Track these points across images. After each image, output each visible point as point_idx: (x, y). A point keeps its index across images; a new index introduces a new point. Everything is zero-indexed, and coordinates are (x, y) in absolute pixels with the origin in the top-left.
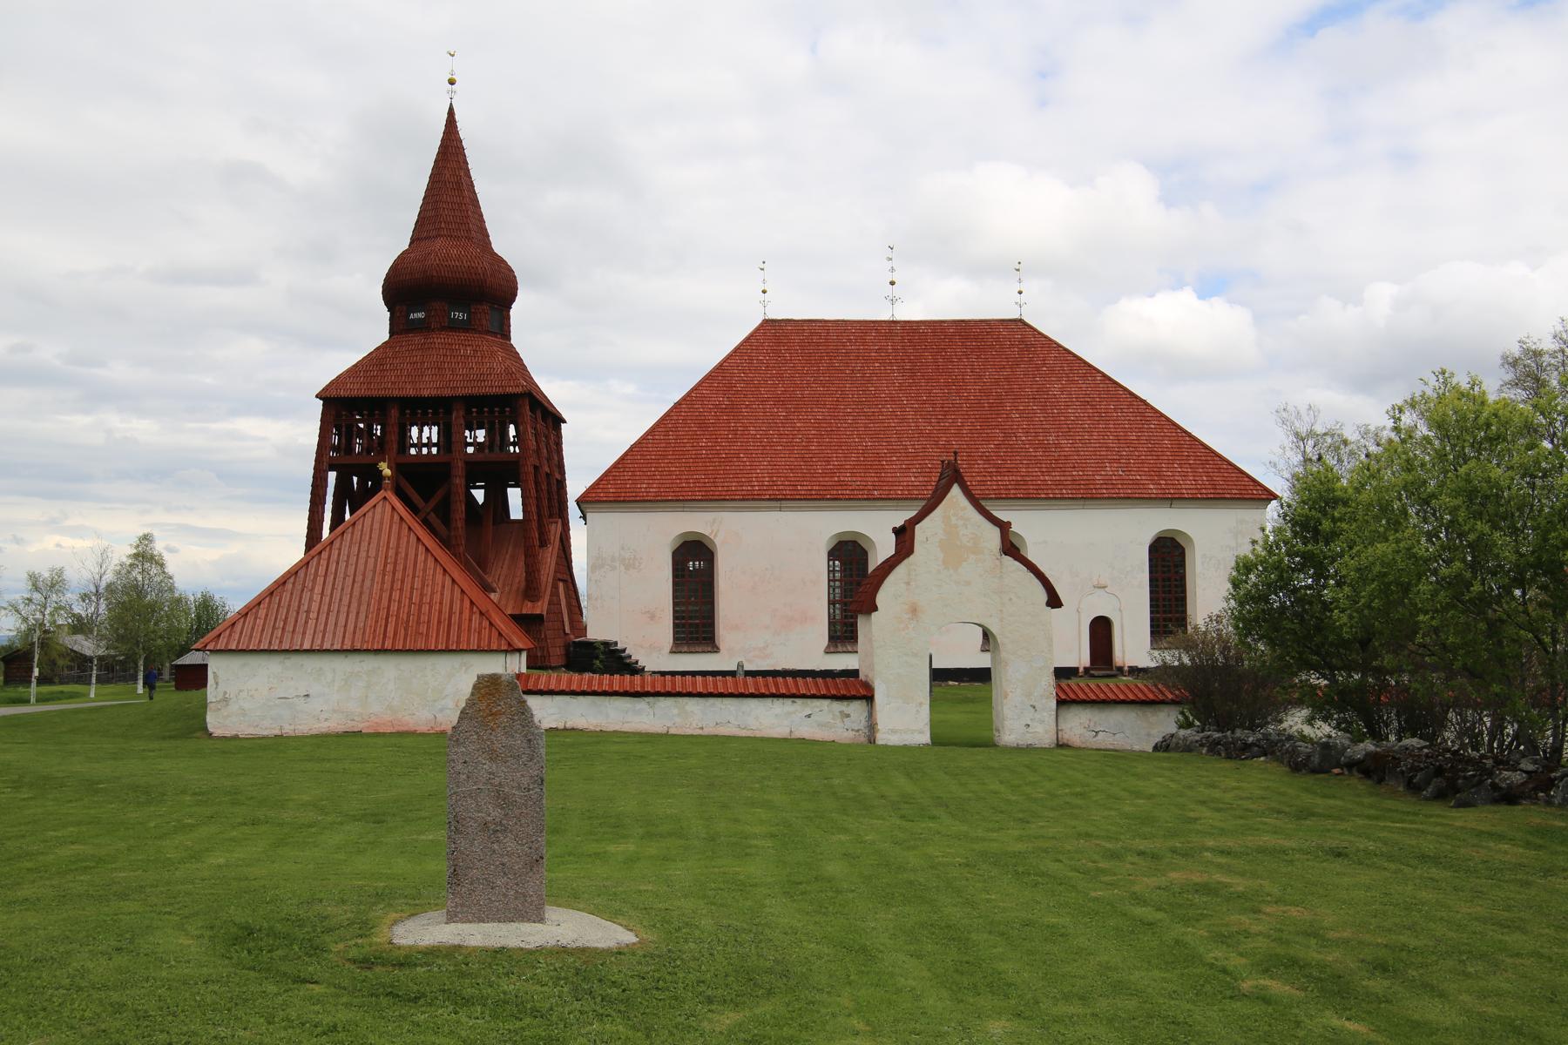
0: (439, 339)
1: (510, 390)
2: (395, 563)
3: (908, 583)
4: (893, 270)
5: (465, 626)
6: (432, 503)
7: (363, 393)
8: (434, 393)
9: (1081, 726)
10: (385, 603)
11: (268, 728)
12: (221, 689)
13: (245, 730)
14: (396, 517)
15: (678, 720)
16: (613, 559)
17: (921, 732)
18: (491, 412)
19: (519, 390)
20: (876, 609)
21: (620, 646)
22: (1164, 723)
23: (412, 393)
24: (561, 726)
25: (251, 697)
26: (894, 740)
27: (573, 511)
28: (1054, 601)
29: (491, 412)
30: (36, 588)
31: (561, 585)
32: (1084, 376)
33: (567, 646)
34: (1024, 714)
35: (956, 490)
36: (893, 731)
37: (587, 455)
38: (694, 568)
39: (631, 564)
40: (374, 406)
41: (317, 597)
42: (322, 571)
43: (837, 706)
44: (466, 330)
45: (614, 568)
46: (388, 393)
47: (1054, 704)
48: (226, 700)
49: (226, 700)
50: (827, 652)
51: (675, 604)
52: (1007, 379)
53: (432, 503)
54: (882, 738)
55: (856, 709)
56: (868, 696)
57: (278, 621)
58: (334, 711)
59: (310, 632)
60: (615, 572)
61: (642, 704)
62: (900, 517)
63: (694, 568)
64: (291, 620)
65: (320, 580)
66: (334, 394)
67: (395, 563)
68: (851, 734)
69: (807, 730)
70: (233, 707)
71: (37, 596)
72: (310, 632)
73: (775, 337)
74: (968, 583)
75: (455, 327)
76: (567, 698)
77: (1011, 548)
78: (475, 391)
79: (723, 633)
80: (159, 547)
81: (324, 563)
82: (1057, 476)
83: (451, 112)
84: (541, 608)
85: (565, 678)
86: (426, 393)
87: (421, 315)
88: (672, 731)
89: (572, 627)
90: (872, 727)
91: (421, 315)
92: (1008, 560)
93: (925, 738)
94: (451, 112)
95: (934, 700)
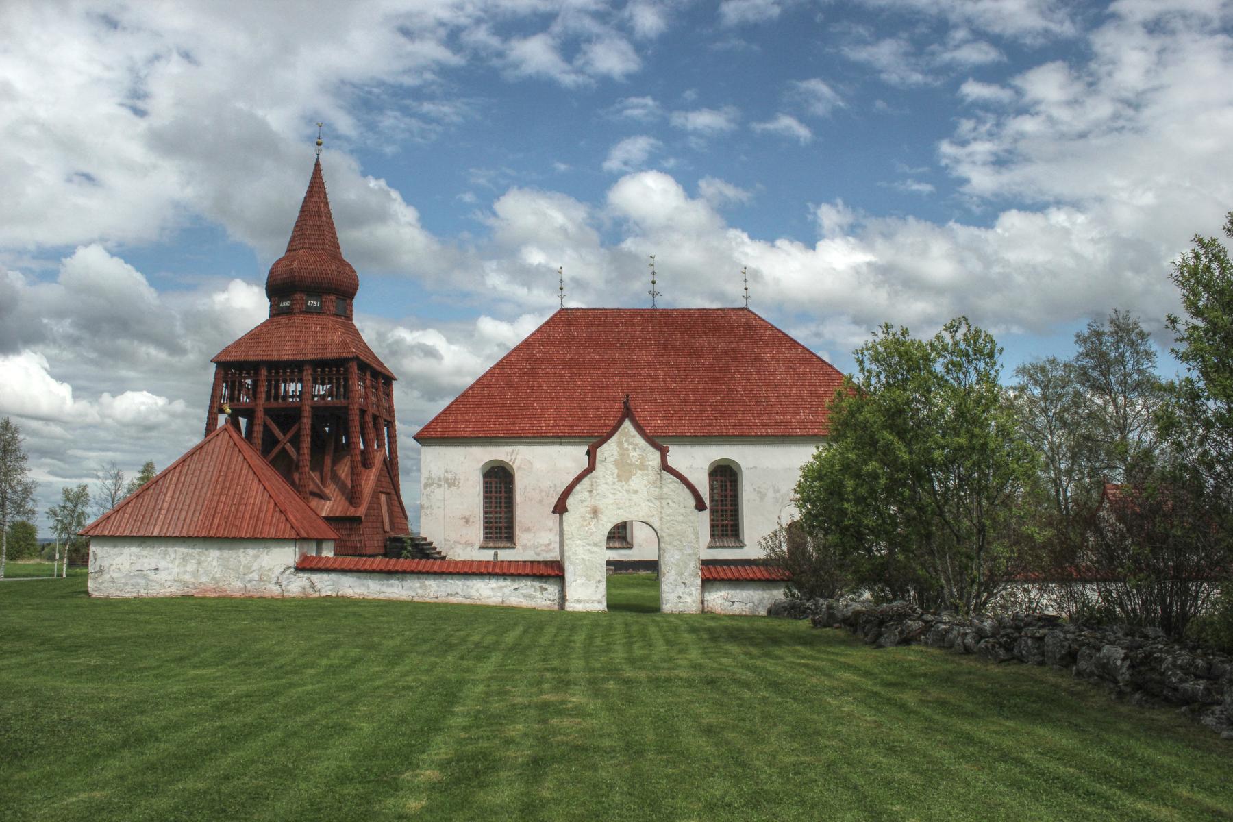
0: (299, 320)
1: (344, 355)
2: (226, 476)
3: (591, 492)
4: (654, 273)
5: (268, 521)
6: (289, 436)
7: (242, 358)
8: (291, 358)
9: (720, 600)
10: (214, 504)
11: (129, 592)
12: (98, 563)
13: (114, 593)
14: (231, 443)
15: (420, 591)
16: (440, 479)
17: (599, 602)
18: (323, 371)
19: (350, 355)
21: (429, 540)
22: (778, 594)
23: (276, 358)
25: (121, 571)
26: (579, 608)
27: (484, 455)
29: (331, 371)
30: (68, 499)
31: (383, 498)
32: (789, 349)
33: (385, 540)
34: (680, 594)
35: (627, 423)
36: (578, 601)
37: (411, 409)
39: (452, 483)
40: (251, 367)
41: (168, 499)
42: (174, 481)
44: (318, 313)
45: (440, 486)
46: (259, 358)
47: (699, 581)
48: (101, 571)
49: (101, 571)
51: (485, 513)
52: (734, 350)
53: (289, 436)
54: (570, 606)
55: (552, 590)
57: (143, 514)
59: (160, 523)
60: (441, 492)
64: (148, 516)
65: (172, 487)
66: (223, 359)
67: (226, 476)
68: (548, 603)
69: (515, 600)
70: (107, 577)
71: (69, 504)
72: (160, 523)
73: (565, 319)
74: (636, 492)
75: (309, 311)
77: (665, 467)
78: (319, 357)
79: (521, 536)
81: (176, 475)
82: (764, 419)
83: (317, 164)
84: (361, 511)
85: (379, 562)
86: (285, 358)
87: (287, 303)
88: (416, 599)
89: (392, 523)
90: (563, 598)
91: (287, 303)
92: (667, 475)
93: (601, 607)
94: (317, 164)
95: (610, 583)
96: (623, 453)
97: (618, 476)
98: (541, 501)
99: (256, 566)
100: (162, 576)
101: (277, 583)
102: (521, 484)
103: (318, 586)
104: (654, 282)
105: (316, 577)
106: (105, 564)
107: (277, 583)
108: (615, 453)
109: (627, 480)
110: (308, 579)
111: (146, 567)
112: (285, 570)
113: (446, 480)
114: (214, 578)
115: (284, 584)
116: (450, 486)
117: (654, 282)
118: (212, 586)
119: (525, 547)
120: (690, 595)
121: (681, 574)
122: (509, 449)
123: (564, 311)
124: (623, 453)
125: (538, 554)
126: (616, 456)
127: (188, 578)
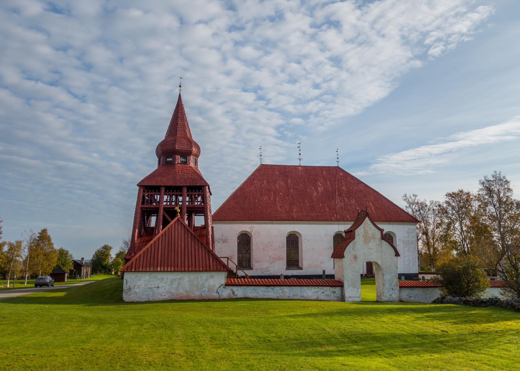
3: (353, 249)
12: (128, 285)
15: (281, 294)
16: (219, 239)
20: (344, 257)
22: (437, 293)
24: (243, 297)
28: (397, 254)
35: (367, 219)
37: (215, 203)
38: (245, 241)
40: (156, 189)
43: (332, 289)
45: (219, 242)
47: (398, 288)
48: (130, 289)
50: (287, 269)
55: (337, 290)
56: (340, 284)
58: (167, 292)
61: (270, 289)
62: (343, 227)
63: (245, 241)
70: (133, 291)
74: (371, 249)
76: (245, 287)
79: (255, 264)
80: (49, 233)
83: (180, 96)
87: (171, 159)
91: (171, 159)
94: (180, 96)
96: (366, 232)
97: (364, 242)
98: (264, 249)
99: (206, 285)
100: (161, 290)
101: (217, 292)
102: (255, 241)
103: (236, 293)
104: (300, 154)
105: (235, 288)
106: (132, 286)
107: (217, 292)
108: (363, 232)
109: (368, 244)
110: (231, 290)
111: (153, 286)
112: (221, 286)
113: (222, 240)
114: (186, 291)
115: (220, 293)
116: (224, 242)
117: (300, 154)
118: (185, 294)
119: (257, 269)
120: (395, 294)
121: (391, 285)
122: (250, 226)
123: (262, 165)
124: (366, 232)
125: (262, 273)
126: (363, 233)
127: (173, 291)
